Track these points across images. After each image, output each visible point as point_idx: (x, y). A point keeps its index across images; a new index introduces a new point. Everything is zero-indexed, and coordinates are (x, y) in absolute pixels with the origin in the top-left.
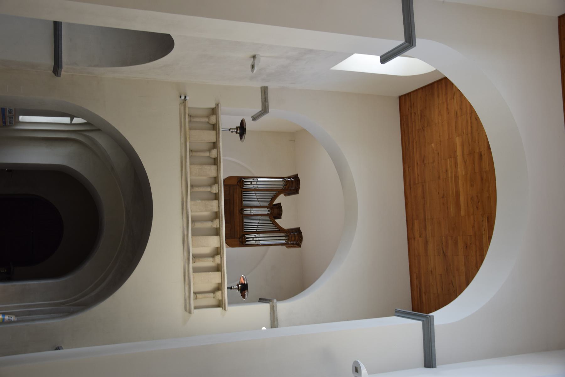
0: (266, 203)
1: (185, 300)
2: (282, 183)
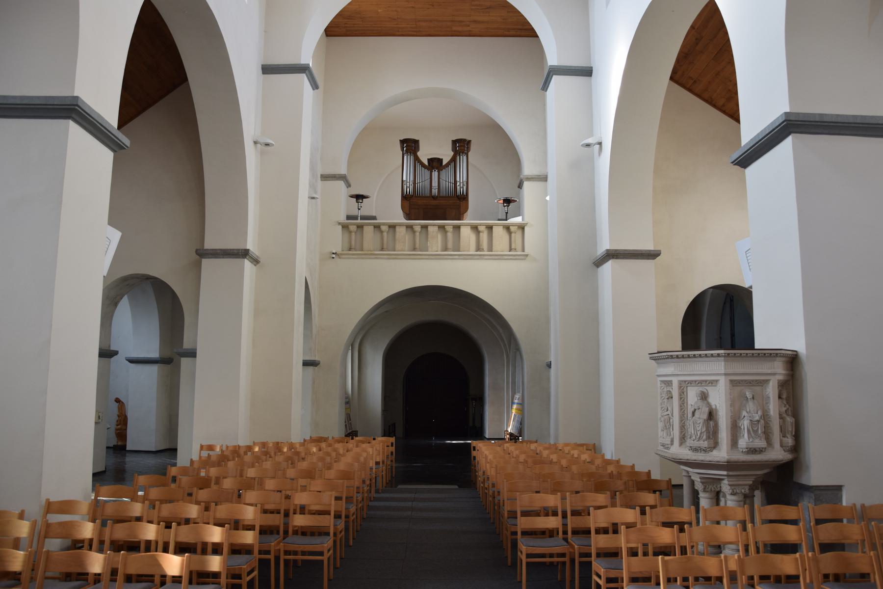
0: (427, 173)
2: (409, 157)
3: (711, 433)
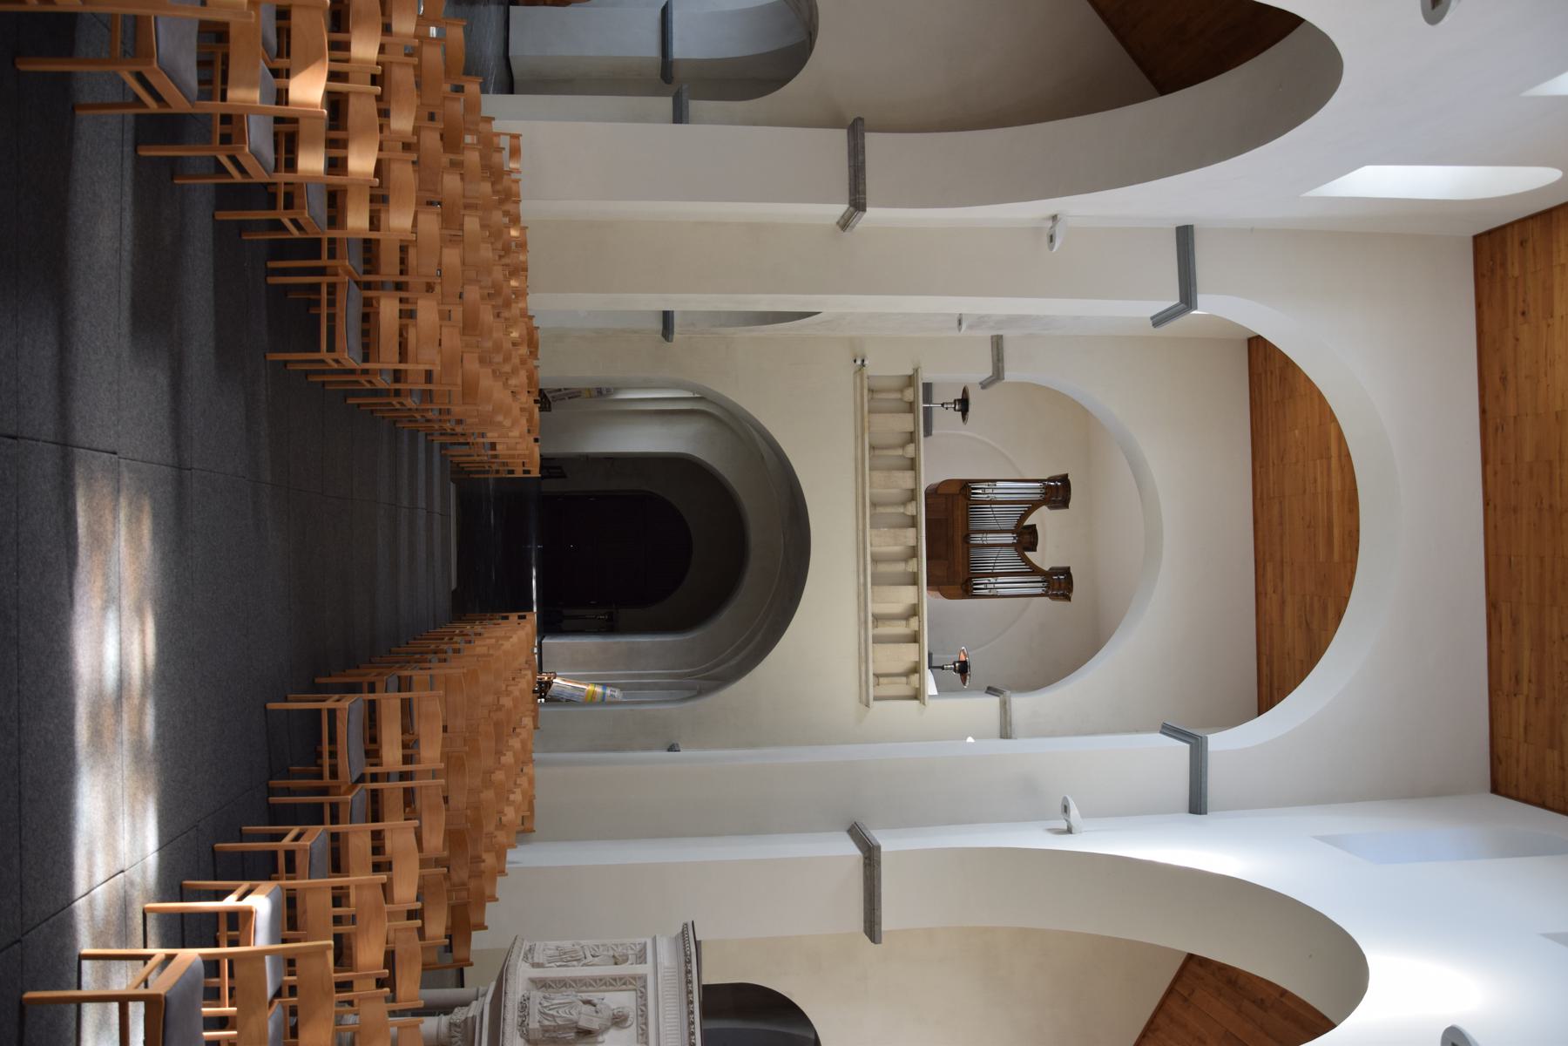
0: (1011, 524)
1: (860, 686)
2: (1038, 491)
3: (554, 1035)
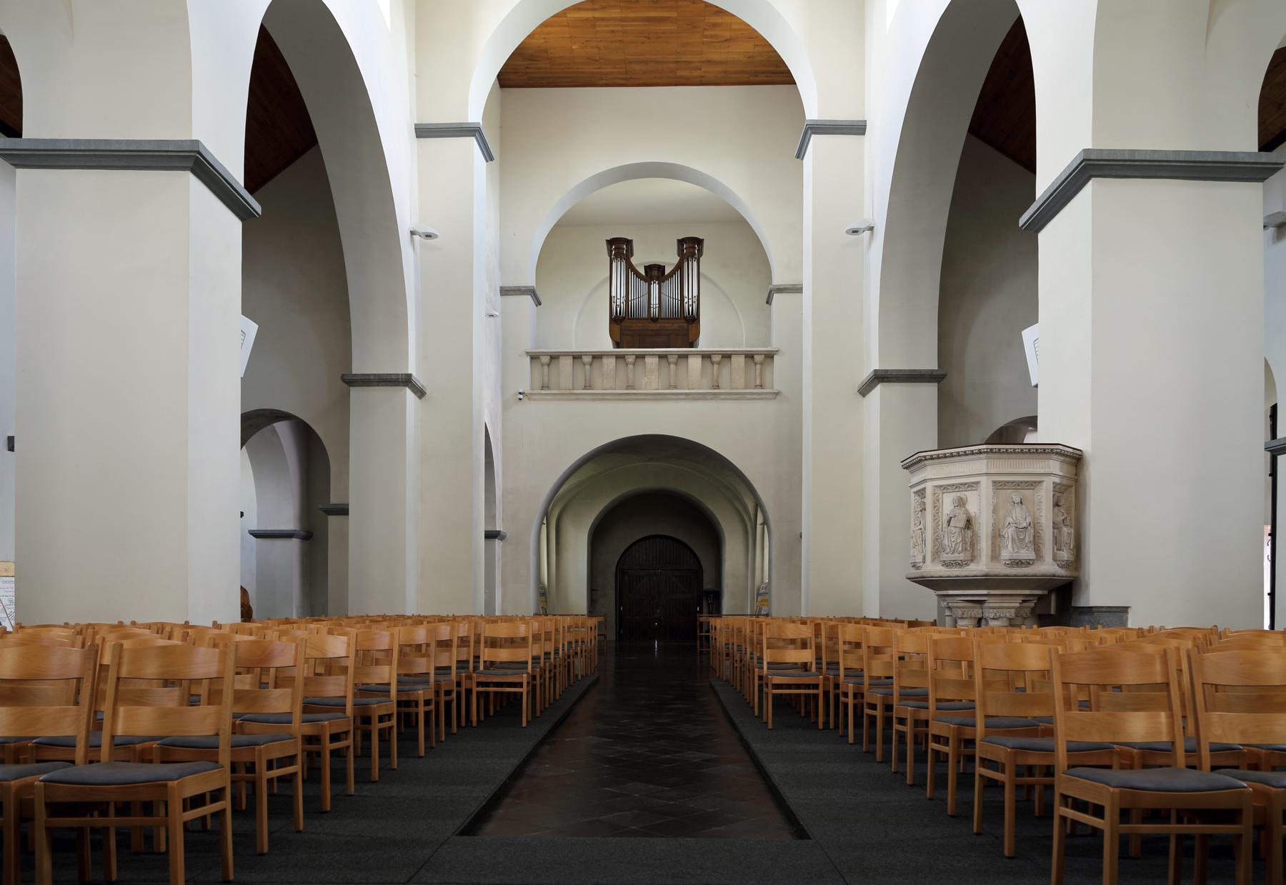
0: (644, 285)
3: (969, 543)
